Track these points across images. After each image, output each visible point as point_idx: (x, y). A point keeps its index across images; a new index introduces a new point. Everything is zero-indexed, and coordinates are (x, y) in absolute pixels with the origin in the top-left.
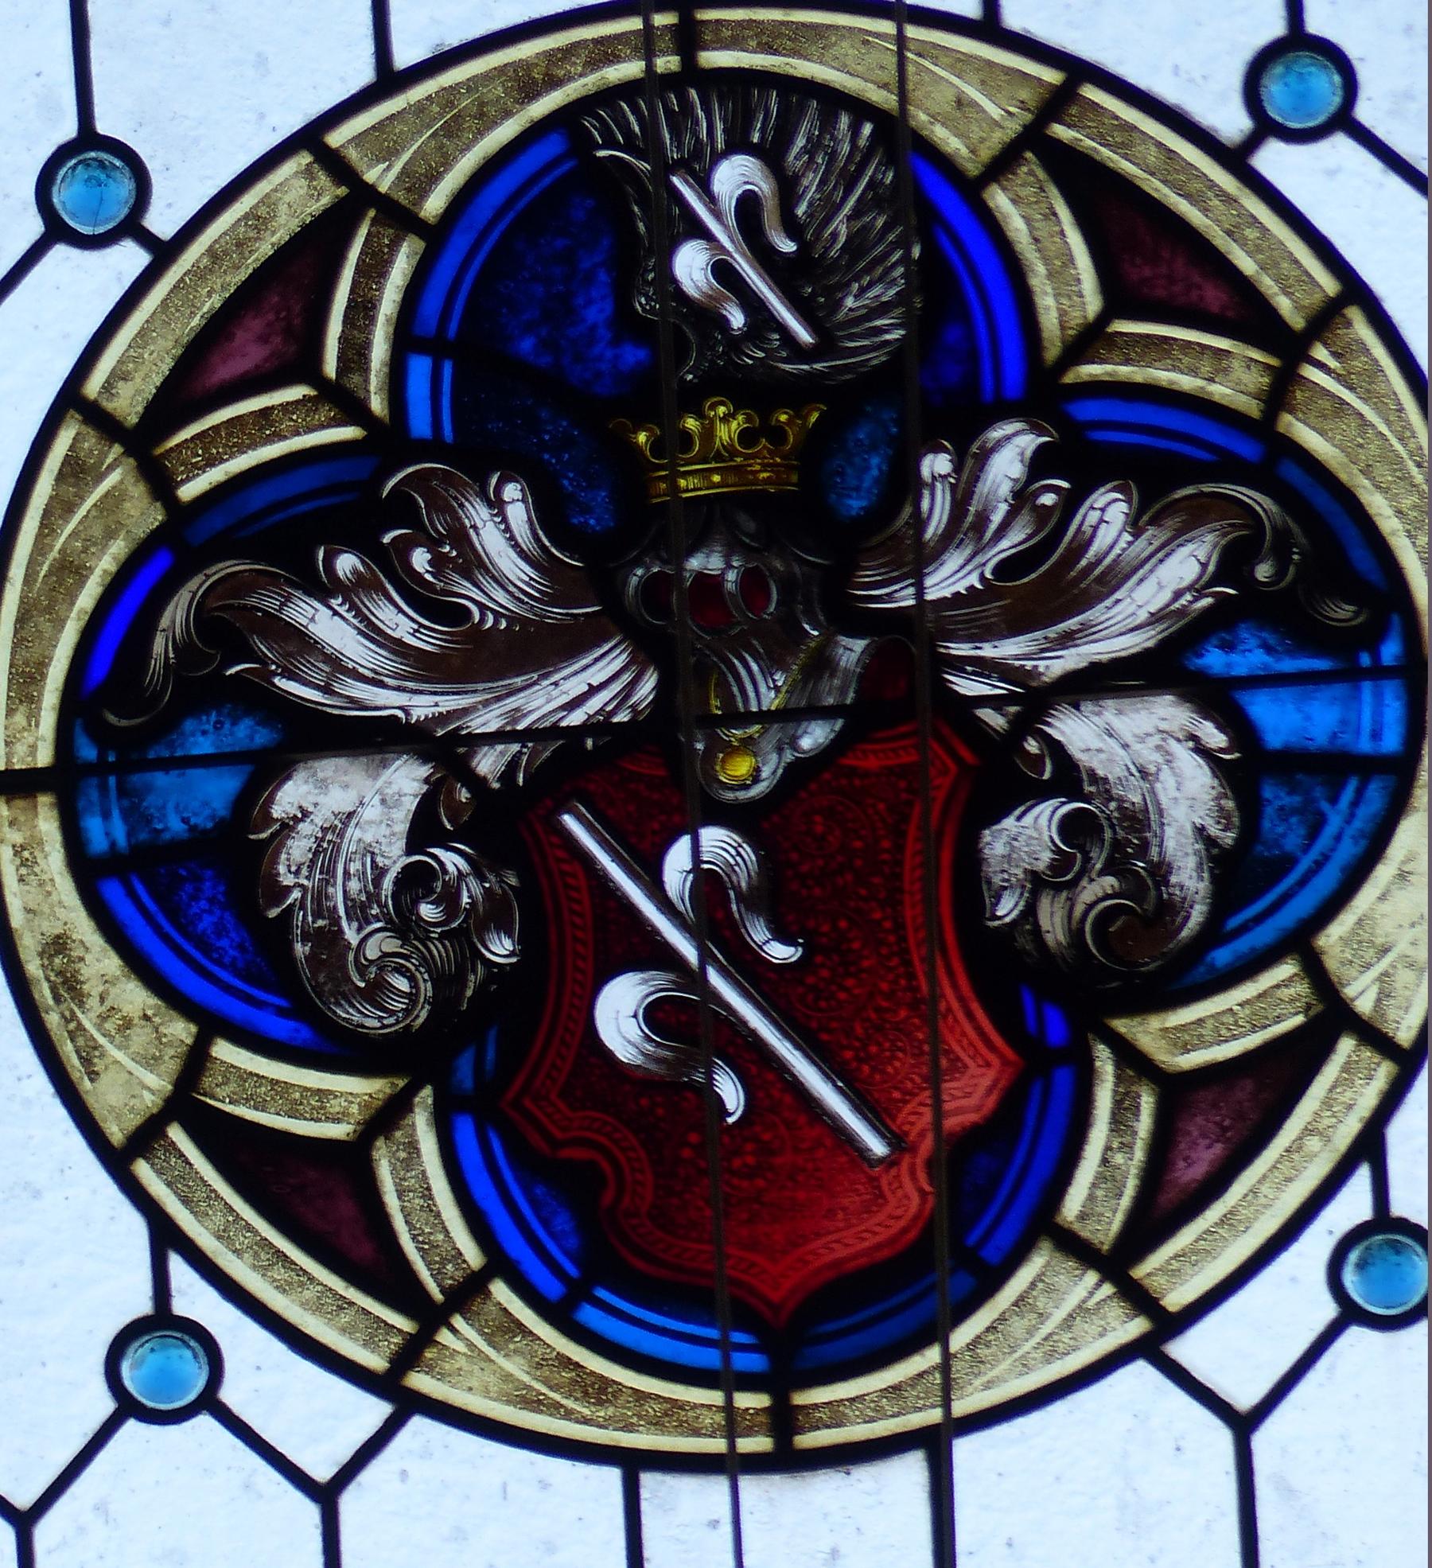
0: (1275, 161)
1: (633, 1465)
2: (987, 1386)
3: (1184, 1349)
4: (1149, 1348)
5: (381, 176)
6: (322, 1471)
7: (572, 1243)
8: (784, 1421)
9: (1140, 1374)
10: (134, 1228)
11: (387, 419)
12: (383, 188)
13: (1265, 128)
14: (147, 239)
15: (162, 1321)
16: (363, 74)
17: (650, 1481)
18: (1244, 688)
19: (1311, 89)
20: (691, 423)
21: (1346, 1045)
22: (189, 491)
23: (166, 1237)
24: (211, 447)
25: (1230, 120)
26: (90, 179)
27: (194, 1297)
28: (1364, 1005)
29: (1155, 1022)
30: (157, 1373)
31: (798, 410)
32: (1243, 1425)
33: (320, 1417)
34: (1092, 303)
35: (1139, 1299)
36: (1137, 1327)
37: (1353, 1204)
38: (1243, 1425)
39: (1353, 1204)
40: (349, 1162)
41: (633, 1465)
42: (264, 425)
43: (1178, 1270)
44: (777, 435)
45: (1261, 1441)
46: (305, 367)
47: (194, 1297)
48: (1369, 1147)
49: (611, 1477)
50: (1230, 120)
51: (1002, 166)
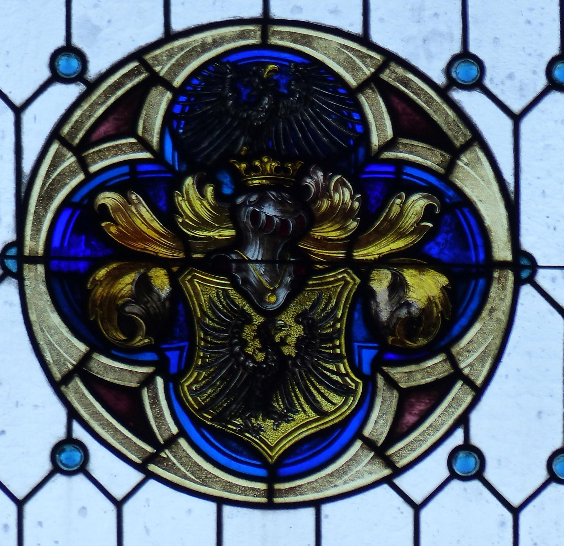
0: (458, 95)
1: (220, 502)
2: (345, 483)
3: (399, 481)
4: (388, 480)
5: (162, 70)
6: (18, 100)
7: (251, 273)
8: (271, 493)
9: (385, 488)
10: (61, 413)
11: (154, 368)
12: (162, 74)
13: (452, 83)
14: (85, 82)
15: (69, 441)
16: (157, 32)
17: (227, 510)
18: (263, 477)
19: (465, 72)
20: (257, 163)
21: (459, 384)
22: (93, 169)
23: (73, 415)
24: (101, 155)
25: (440, 79)
26: (66, 64)
27: (79, 432)
28: (466, 371)
29: (400, 369)
30: (67, 459)
31: (293, 161)
32: (417, 508)
33: (119, 476)
34: (390, 133)
35: (388, 462)
36: (386, 472)
37: (458, 438)
38: (417, 508)
39: (458, 438)
40: (133, 395)
41: (220, 502)
42: (119, 150)
43: (402, 452)
44: (287, 170)
45: (424, 514)
46: (134, 134)
47: (79, 432)
48: (463, 421)
49: (212, 506)
50: (440, 79)
51: (363, 86)
